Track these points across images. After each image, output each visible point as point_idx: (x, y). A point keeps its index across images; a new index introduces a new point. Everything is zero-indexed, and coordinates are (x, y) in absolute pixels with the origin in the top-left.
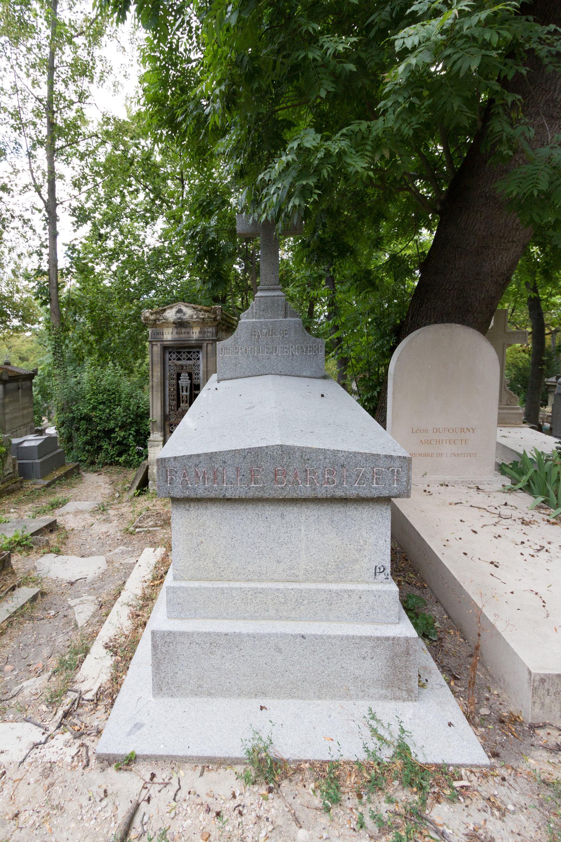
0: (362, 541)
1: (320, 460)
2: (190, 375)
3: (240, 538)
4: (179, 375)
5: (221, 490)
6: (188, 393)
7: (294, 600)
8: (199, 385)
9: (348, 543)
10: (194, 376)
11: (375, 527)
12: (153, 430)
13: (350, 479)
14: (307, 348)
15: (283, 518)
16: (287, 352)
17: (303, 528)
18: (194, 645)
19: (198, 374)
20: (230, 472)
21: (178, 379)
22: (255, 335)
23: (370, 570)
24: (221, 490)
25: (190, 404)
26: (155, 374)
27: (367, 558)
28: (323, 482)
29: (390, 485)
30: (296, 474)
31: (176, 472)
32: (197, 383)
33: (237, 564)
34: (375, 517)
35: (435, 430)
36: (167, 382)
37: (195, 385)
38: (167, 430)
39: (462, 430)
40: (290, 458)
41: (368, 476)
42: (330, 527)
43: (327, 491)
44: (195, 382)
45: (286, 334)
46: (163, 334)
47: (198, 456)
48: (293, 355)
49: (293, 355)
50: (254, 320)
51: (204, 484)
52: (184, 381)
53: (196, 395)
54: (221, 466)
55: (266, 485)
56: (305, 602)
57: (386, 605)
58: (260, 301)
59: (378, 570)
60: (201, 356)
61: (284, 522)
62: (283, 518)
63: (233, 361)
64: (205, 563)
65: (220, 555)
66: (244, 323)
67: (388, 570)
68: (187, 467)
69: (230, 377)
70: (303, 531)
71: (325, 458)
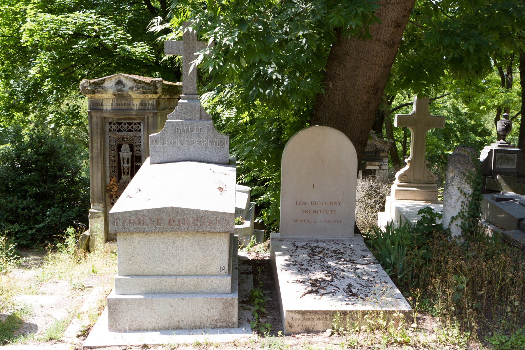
2: (131, 147)
4: (119, 147)
6: (129, 165)
10: (135, 148)
11: (220, 248)
12: (94, 202)
16: (201, 145)
17: (184, 248)
18: (129, 305)
19: (140, 146)
20: (147, 220)
21: (119, 150)
22: (178, 131)
25: (132, 176)
30: (179, 221)
32: (138, 155)
36: (107, 154)
37: (136, 156)
38: (108, 201)
39: (332, 203)
44: (137, 154)
45: (201, 131)
46: (102, 105)
47: (131, 212)
48: (206, 147)
49: (206, 147)
50: (178, 120)
52: (125, 153)
53: (138, 168)
58: (182, 106)
60: (142, 127)
63: (162, 150)
66: (170, 122)
67: (227, 269)
69: (159, 161)
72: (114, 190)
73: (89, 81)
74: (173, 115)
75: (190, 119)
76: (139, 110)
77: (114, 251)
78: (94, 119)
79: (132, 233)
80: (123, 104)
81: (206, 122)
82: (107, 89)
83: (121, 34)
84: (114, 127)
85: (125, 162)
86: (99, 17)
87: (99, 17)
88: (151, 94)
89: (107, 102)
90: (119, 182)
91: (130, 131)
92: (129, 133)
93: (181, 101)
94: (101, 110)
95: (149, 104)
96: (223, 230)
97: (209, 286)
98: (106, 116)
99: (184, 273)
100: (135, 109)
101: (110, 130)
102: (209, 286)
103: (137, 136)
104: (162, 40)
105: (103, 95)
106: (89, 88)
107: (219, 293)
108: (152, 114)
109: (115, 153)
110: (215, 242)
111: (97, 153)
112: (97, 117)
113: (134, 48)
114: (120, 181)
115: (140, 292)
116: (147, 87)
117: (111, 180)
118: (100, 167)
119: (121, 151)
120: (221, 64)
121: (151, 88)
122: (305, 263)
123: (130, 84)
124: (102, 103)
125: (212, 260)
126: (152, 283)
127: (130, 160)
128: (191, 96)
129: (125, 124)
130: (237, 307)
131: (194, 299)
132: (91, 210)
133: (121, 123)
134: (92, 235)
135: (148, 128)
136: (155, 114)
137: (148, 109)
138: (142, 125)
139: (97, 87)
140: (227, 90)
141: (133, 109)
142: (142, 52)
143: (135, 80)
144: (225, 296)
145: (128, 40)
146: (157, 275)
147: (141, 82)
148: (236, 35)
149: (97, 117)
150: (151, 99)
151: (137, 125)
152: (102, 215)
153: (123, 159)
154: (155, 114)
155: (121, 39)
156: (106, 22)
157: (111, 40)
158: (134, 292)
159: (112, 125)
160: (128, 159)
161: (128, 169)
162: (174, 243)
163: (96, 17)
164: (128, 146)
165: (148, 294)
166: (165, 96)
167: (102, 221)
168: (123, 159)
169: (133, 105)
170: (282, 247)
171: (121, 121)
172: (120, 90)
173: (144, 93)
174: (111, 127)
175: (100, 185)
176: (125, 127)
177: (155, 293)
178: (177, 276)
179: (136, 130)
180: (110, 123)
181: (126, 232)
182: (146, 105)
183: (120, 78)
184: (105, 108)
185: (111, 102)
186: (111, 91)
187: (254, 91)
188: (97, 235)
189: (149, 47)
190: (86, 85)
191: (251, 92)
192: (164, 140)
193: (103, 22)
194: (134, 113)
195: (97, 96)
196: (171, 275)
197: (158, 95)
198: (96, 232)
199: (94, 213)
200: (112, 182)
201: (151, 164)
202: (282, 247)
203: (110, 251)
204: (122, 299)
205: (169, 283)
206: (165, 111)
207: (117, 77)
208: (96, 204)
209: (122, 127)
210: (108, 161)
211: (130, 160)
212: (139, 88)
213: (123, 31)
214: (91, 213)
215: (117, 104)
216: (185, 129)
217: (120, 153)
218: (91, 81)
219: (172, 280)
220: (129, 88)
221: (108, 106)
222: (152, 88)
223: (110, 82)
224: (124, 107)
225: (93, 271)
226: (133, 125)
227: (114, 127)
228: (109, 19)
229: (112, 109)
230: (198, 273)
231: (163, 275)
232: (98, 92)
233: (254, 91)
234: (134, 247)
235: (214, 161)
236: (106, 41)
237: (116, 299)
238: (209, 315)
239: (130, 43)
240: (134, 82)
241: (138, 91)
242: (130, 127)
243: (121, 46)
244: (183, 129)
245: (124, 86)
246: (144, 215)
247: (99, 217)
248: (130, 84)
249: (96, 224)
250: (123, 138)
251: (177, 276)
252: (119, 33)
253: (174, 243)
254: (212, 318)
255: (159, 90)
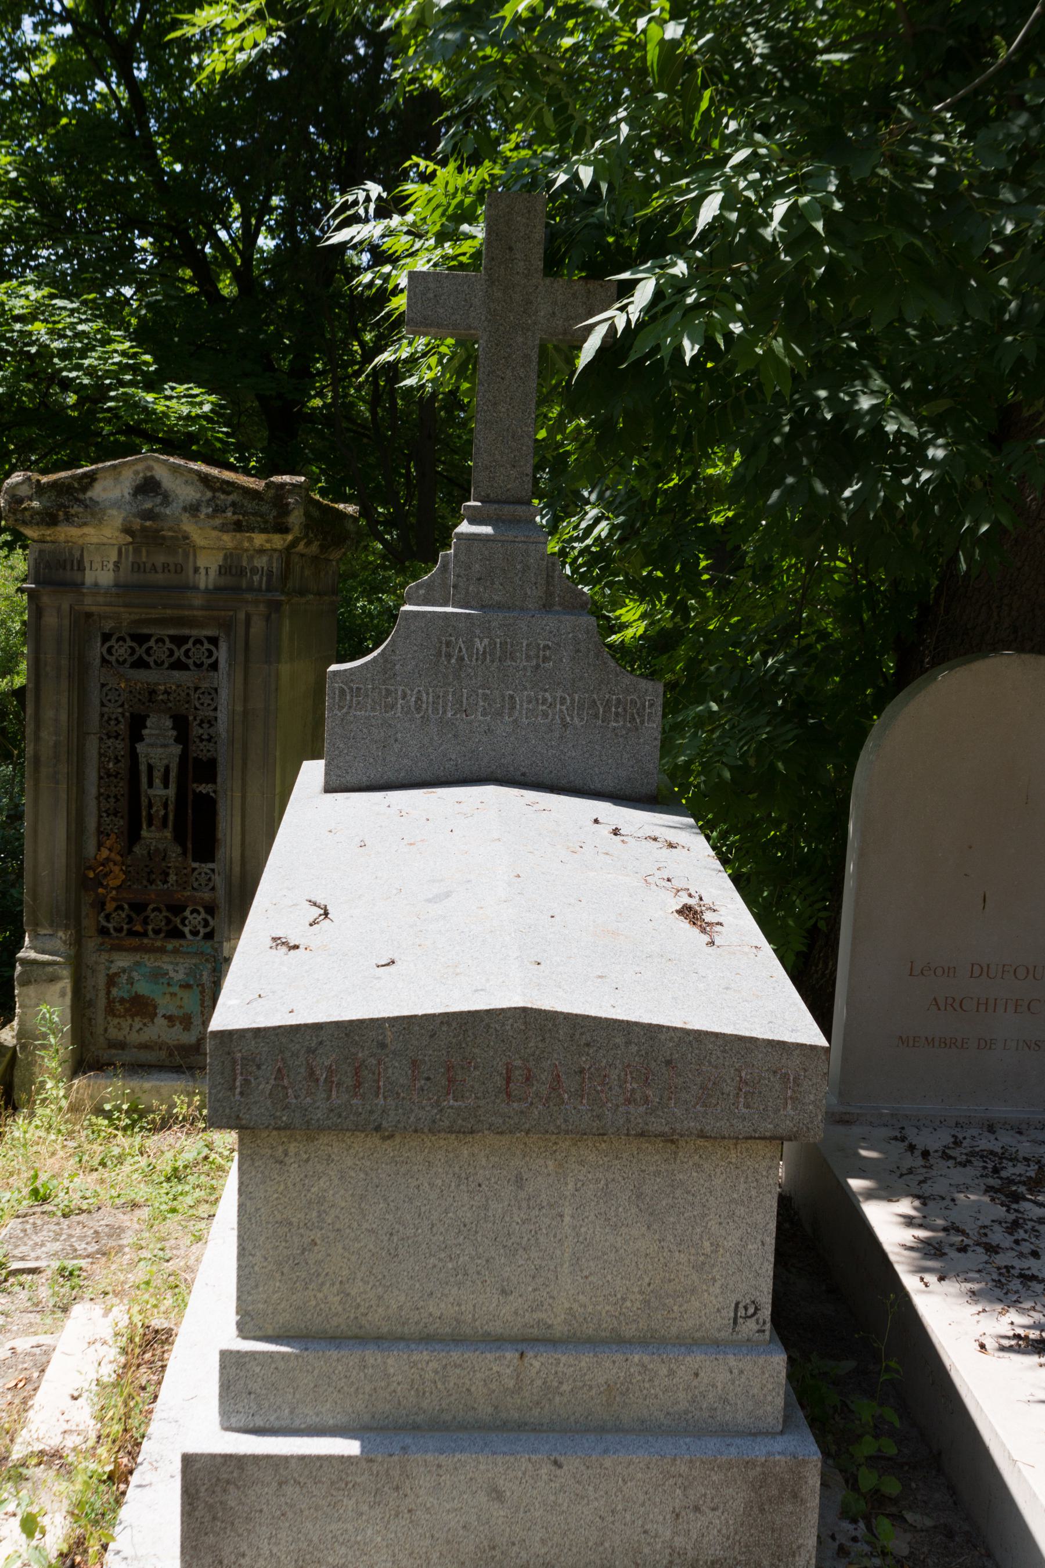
0: (707, 1244)
1: (617, 1047)
2: (181, 725)
3: (410, 1232)
4: (137, 725)
5: (371, 1112)
6: (171, 792)
7: (539, 1382)
8: (212, 763)
9: (674, 1247)
10: (196, 731)
11: (741, 1211)
12: (36, 924)
13: (684, 1096)
14: (607, 704)
15: (521, 1188)
16: (545, 715)
17: (567, 1211)
18: (289, 1490)
19: (212, 722)
22: (449, 656)
23: (724, 1313)
24: (371, 1112)
26: (48, 714)
27: (718, 1284)
28: (621, 1099)
29: (777, 1111)
31: (259, 1067)
33: (402, 1298)
34: (742, 1187)
35: (977, 970)
40: (543, 1040)
41: (726, 1090)
42: (634, 1210)
43: (628, 1121)
44: (200, 750)
45: (546, 659)
46: (81, 568)
48: (565, 726)
49: (565, 726)
50: (449, 609)
51: (328, 1098)
52: (159, 749)
54: (373, 1055)
55: (482, 1103)
56: (565, 1387)
57: (756, 1391)
59: (741, 1312)
60: (222, 655)
61: (522, 1195)
62: (521, 1188)
64: (320, 1295)
65: (359, 1275)
67: (766, 1312)
68: (288, 1054)
70: (567, 1219)
71: (628, 1043)
72: (114, 883)
73: (35, 476)
74: (429, 585)
75: (500, 607)
76: (218, 589)
77: (107, 1107)
78: (50, 620)
79: (311, 1130)
80: (159, 566)
81: (568, 621)
82: (103, 511)
83: (124, 354)
84: (121, 651)
85: (157, 782)
86: (52, 296)
87: (52, 296)
88: (263, 531)
89: (97, 559)
90: (130, 851)
91: (179, 666)
92: (176, 674)
93: (465, 527)
94: (77, 586)
95: (254, 570)
96: (767, 1127)
97: (681, 1395)
98: (94, 609)
99: (560, 1329)
100: (202, 586)
101: (104, 660)
102: (681, 1395)
103: (205, 685)
104: (378, 282)
105: (86, 530)
106: (35, 504)
107: (726, 1432)
108: (262, 608)
109: (120, 746)
110: (718, 1182)
111: (56, 745)
112: (59, 610)
113: (163, 402)
114: (136, 849)
115: (341, 1419)
116: (250, 505)
117: (100, 845)
118: (64, 796)
119: (141, 739)
120: (737, 328)
121: (264, 508)
122: (998, 1236)
123: (186, 492)
124: (81, 562)
125: (699, 1268)
126: (401, 1375)
127: (173, 774)
128: (508, 509)
129: (159, 640)
130: (814, 1502)
131: (608, 1463)
132: (27, 953)
133: (148, 637)
134: (24, 1047)
135: (247, 660)
136: (275, 607)
137: (250, 589)
138: (223, 646)
139: (64, 500)
140: (593, 513)
141: (195, 588)
142: (188, 417)
143: (205, 480)
144: (759, 1450)
145: (144, 374)
146: (428, 1340)
147: (229, 487)
148: (832, 188)
149: (59, 610)
150: (261, 551)
151: (207, 645)
152: (65, 973)
153: (150, 768)
154: (275, 607)
155: (123, 368)
156: (72, 311)
157: (91, 371)
158: (313, 1420)
159: (113, 642)
160: (167, 769)
161: (166, 806)
162: (519, 1181)
163: (40, 294)
164: (169, 723)
165: (381, 1429)
166: (308, 544)
167: (63, 994)
168: (150, 768)
169: (196, 570)
170: (864, 1153)
171: (146, 631)
172: (149, 515)
173: (239, 527)
174: (109, 651)
175: (61, 862)
176: (160, 652)
177: (416, 1427)
178: (525, 1342)
179: (199, 666)
180: (106, 637)
181: (287, 1127)
182: (242, 572)
183: (150, 468)
184: (89, 577)
185: (114, 557)
186: (116, 518)
187: (789, 491)
188: (44, 1047)
189: (213, 398)
190: (24, 491)
191: (776, 494)
192: (388, 692)
193: (65, 313)
194: (198, 602)
195: (66, 533)
196: (494, 1341)
197: (290, 537)
198: (44, 1036)
199: (34, 962)
200: (105, 853)
201: (328, 789)
202: (864, 1153)
203: (88, 1105)
204: (256, 1459)
205: (485, 1377)
206: (303, 600)
207: (140, 467)
208: (43, 932)
209: (148, 651)
210: (92, 775)
211: (173, 774)
212: (218, 510)
213: (128, 344)
214: (25, 962)
215: (137, 567)
216: (479, 645)
217: (140, 748)
218: (44, 480)
219: (501, 1364)
220: (185, 509)
221: (100, 574)
222: (272, 511)
223: (114, 485)
224: (160, 578)
225: (35, 1192)
226: (190, 645)
227: (121, 651)
228: (84, 303)
229: (117, 585)
230: (629, 1331)
231: (457, 1340)
232: (69, 519)
233: (789, 491)
234: (321, 1200)
235: (598, 786)
236: (74, 374)
237: (227, 1458)
238: (679, 1541)
239: (152, 384)
240: (201, 487)
241: (218, 522)
242: (179, 653)
243: (122, 390)
244: (470, 644)
245: (167, 499)
246: (383, 1045)
247: (53, 979)
248: (186, 492)
249: (44, 1009)
250: (153, 692)
251: (525, 1342)
252: (116, 351)
253: (519, 1181)
254: (691, 1554)
255: (296, 518)
